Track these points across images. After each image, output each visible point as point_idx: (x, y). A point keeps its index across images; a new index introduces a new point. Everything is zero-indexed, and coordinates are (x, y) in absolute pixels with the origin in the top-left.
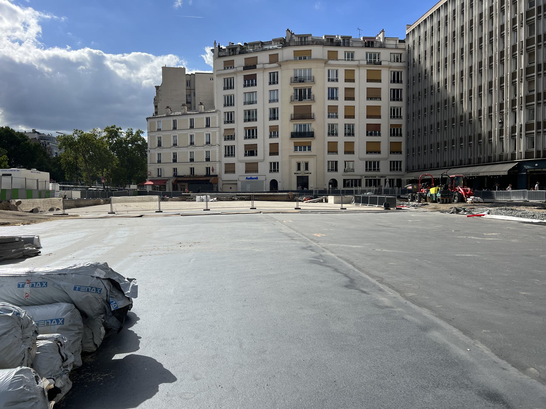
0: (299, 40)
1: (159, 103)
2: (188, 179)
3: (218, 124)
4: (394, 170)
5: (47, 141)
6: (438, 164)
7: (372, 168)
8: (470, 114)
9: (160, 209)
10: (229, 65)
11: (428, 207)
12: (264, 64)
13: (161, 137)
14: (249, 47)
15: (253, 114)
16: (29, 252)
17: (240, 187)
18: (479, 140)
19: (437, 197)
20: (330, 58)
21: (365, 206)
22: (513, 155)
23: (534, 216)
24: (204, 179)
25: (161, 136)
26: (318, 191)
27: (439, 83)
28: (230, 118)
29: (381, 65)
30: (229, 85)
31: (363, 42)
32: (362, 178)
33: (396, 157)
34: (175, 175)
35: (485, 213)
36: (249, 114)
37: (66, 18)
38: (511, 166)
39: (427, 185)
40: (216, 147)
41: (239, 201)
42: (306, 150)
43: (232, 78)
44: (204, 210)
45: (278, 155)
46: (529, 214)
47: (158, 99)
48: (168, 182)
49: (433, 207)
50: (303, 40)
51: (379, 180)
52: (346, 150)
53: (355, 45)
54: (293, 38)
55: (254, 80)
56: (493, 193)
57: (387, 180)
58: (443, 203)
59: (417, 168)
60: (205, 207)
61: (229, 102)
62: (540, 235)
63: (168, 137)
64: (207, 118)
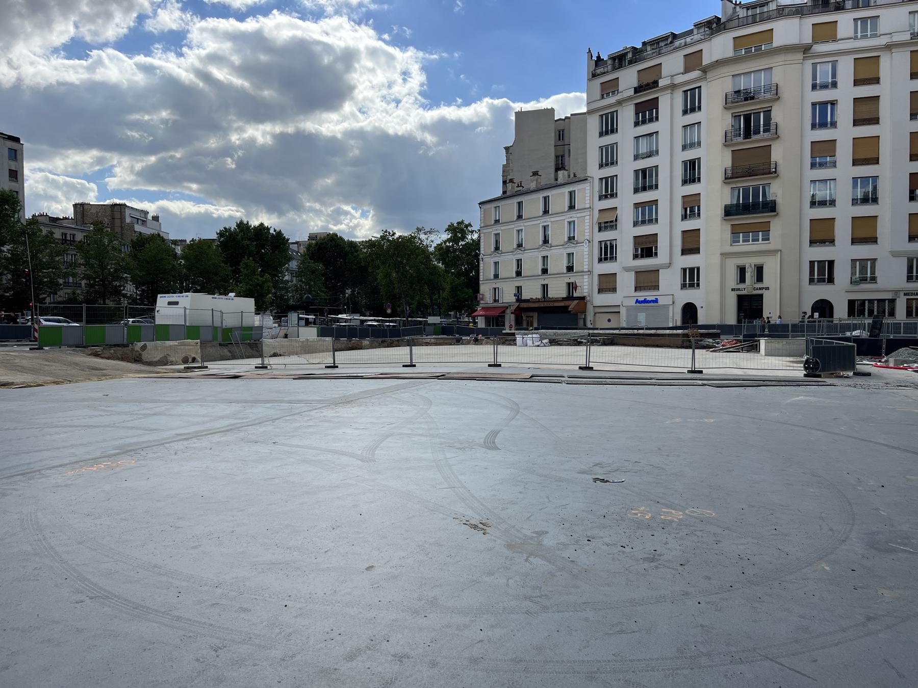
2: (536, 305)
15: (651, 176)
17: (625, 319)
20: (816, 40)
24: (562, 304)
32: (899, 297)
34: (519, 300)
36: (644, 177)
37: (460, 53)
40: (584, 244)
42: (758, 240)
45: (699, 253)
47: (507, 169)
52: (855, 236)
60: (583, 363)
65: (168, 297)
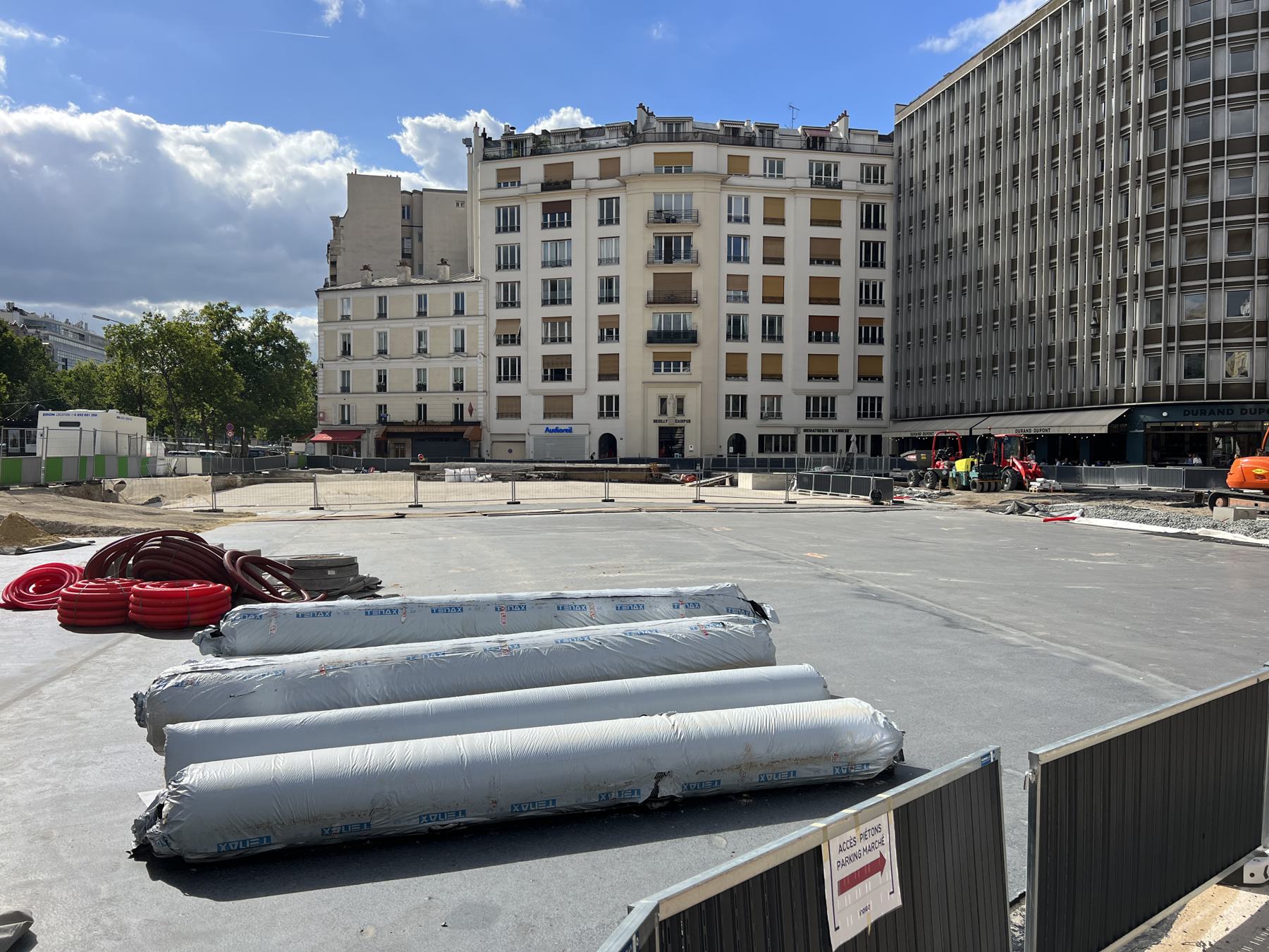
0: (664, 128)
1: (340, 254)
3: (482, 308)
4: (865, 415)
5: (43, 332)
6: (962, 405)
7: (820, 411)
8: (1031, 304)
9: (416, 500)
10: (509, 178)
11: (957, 500)
12: (587, 179)
13: (349, 335)
14: (552, 139)
16: (370, 581)
17: (532, 449)
18: (1049, 358)
19: (970, 478)
20: (731, 172)
21: (822, 496)
22: (1118, 394)
23: (1167, 520)
24: (451, 430)
25: (351, 332)
26: (711, 460)
27: (965, 234)
28: (509, 298)
29: (841, 188)
30: (508, 221)
31: (803, 137)
33: (869, 389)
34: (382, 420)
35: (1076, 514)
36: (554, 288)
37: (64, 38)
38: (1117, 414)
39: (947, 453)
41: (541, 480)
43: (516, 208)
44: (508, 503)
45: (618, 379)
46: (1159, 517)
47: (338, 246)
48: (365, 436)
49: (965, 499)
50: (674, 131)
51: (834, 438)
52: (767, 372)
53: (785, 143)
54: (652, 123)
55: (566, 214)
56: (1080, 470)
57: (853, 438)
58: (982, 491)
59: (916, 412)
60: (509, 497)
61: (509, 259)
62: (1186, 556)
63: (366, 334)
64: (457, 295)
65: (59, 415)
